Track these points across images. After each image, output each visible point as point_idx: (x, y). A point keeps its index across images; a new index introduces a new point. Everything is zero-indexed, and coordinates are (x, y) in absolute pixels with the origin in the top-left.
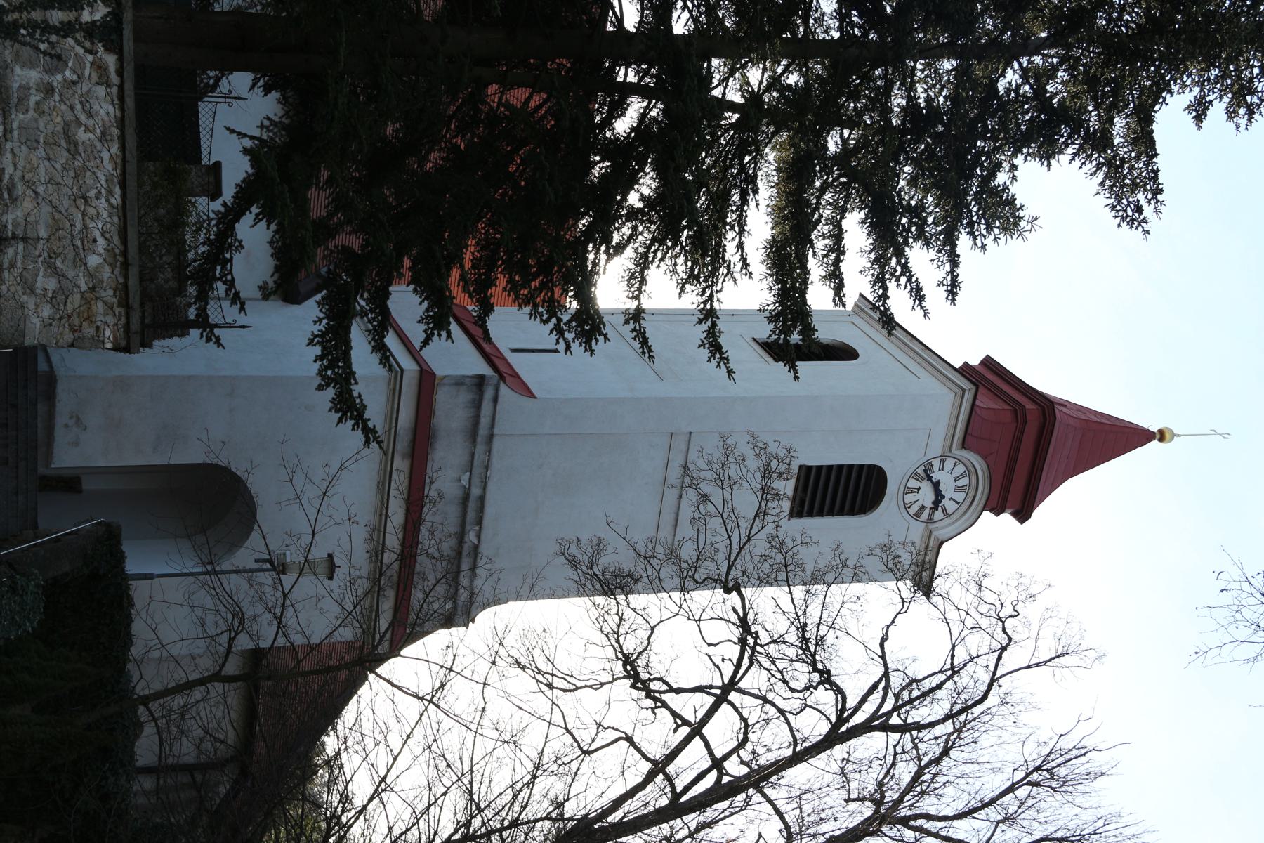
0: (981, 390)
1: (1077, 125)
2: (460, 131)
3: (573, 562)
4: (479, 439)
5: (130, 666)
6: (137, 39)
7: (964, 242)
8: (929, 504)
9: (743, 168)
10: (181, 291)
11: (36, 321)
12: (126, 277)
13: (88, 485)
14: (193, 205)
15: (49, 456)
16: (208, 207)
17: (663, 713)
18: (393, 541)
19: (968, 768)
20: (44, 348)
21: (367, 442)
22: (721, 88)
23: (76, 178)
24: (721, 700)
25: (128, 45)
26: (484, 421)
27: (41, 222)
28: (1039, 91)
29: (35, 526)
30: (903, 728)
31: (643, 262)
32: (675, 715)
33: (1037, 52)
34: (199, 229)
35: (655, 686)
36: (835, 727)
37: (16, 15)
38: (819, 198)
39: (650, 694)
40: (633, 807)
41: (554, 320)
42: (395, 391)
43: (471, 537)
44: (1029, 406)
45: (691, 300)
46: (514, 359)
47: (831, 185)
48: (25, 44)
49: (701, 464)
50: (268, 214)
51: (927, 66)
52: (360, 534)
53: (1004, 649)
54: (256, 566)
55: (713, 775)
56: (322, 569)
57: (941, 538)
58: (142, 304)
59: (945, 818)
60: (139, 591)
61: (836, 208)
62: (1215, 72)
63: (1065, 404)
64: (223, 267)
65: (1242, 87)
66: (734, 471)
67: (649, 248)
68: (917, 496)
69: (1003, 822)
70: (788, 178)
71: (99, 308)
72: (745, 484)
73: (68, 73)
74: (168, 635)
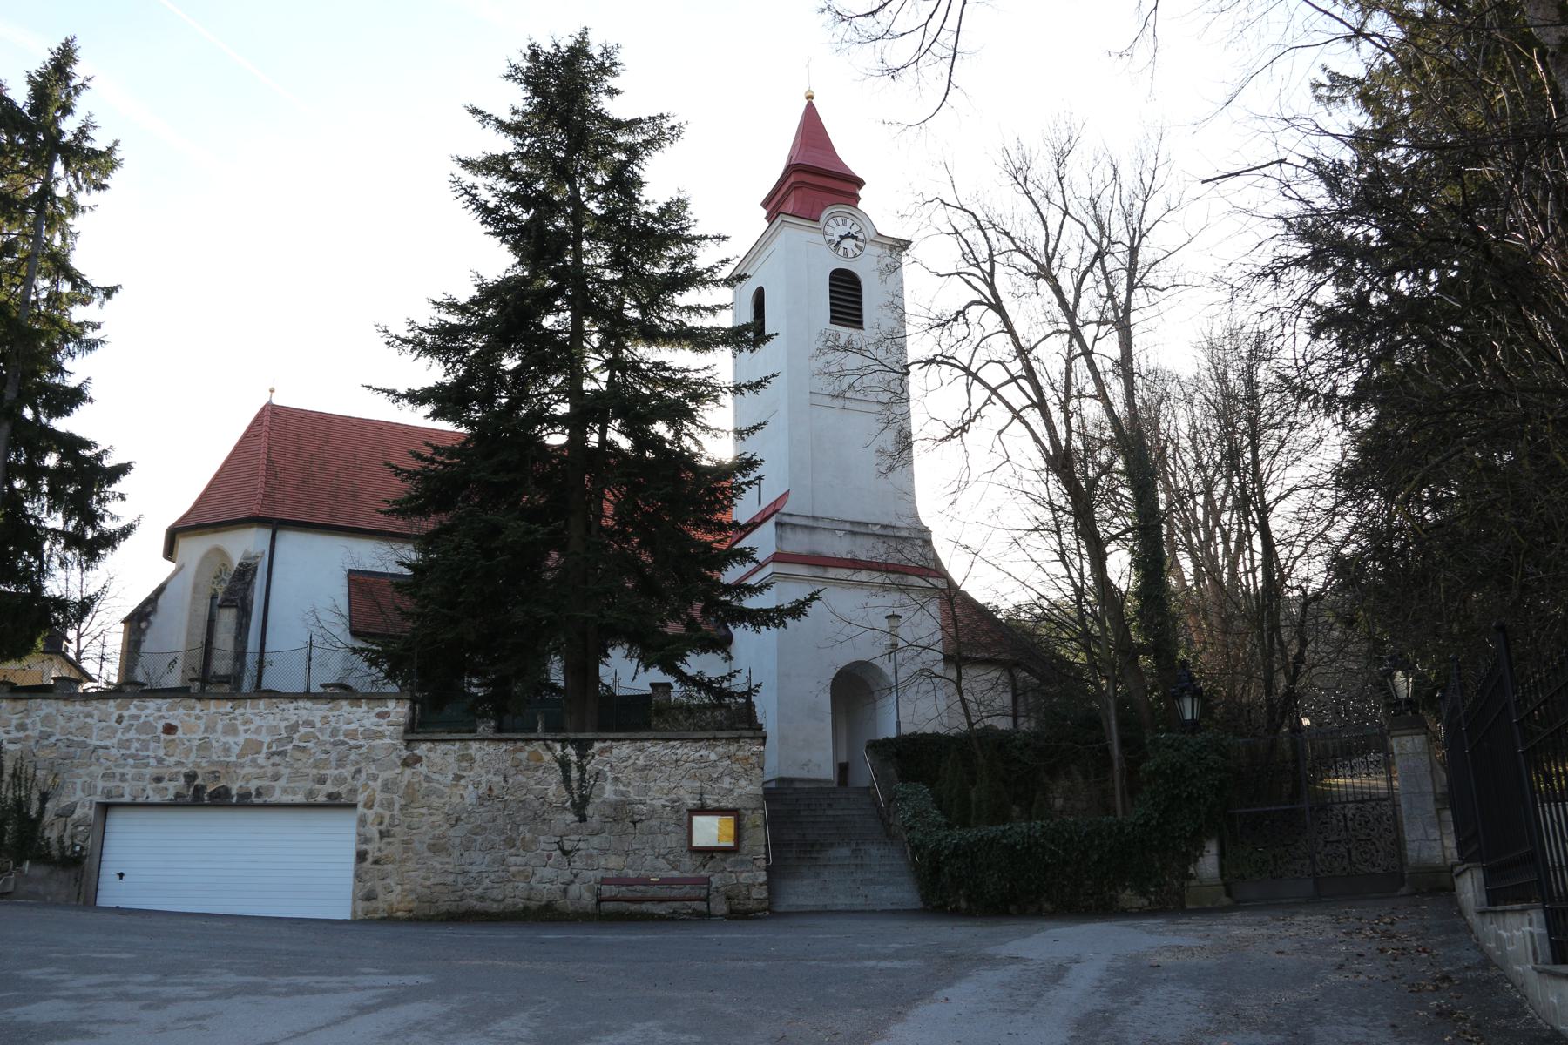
0: (782, 209)
1: (624, 165)
2: (629, 542)
3: (891, 469)
4: (815, 525)
5: (951, 734)
6: (584, 731)
7: (693, 232)
8: (854, 242)
9: (650, 370)
10: (728, 707)
11: (748, 788)
12: (722, 739)
13: (843, 759)
14: (676, 699)
15: (827, 781)
16: (677, 690)
17: (983, 412)
18: (877, 577)
19: (1017, 220)
20: (764, 783)
21: (818, 599)
22: (601, 384)
23: (665, 766)
24: (975, 377)
25: (588, 736)
26: (804, 522)
27: (692, 785)
28: (601, 189)
29: (868, 788)
30: (991, 260)
31: (705, 428)
32: (985, 404)
33: (578, 191)
34: (691, 696)
35: (967, 417)
36: (990, 306)
37: (575, 796)
38: (666, 322)
39: (972, 420)
40: (1041, 430)
41: (743, 486)
42: (786, 577)
43: (876, 529)
44: (792, 180)
45: (727, 399)
46: (765, 503)
47: (658, 314)
48: (591, 792)
49: (831, 388)
50: (682, 657)
51: (585, 257)
52: (874, 601)
53: (942, 202)
54: (892, 663)
55: (1021, 381)
56: (894, 622)
58: (737, 730)
59: (1047, 235)
60: (907, 729)
61: (672, 310)
62: (591, 85)
63: (791, 158)
64: (714, 682)
65: (600, 69)
66: (834, 369)
67: (698, 426)
69: (1048, 199)
70: (655, 342)
71: (740, 754)
72: (842, 362)
73: (606, 769)
74: (932, 713)
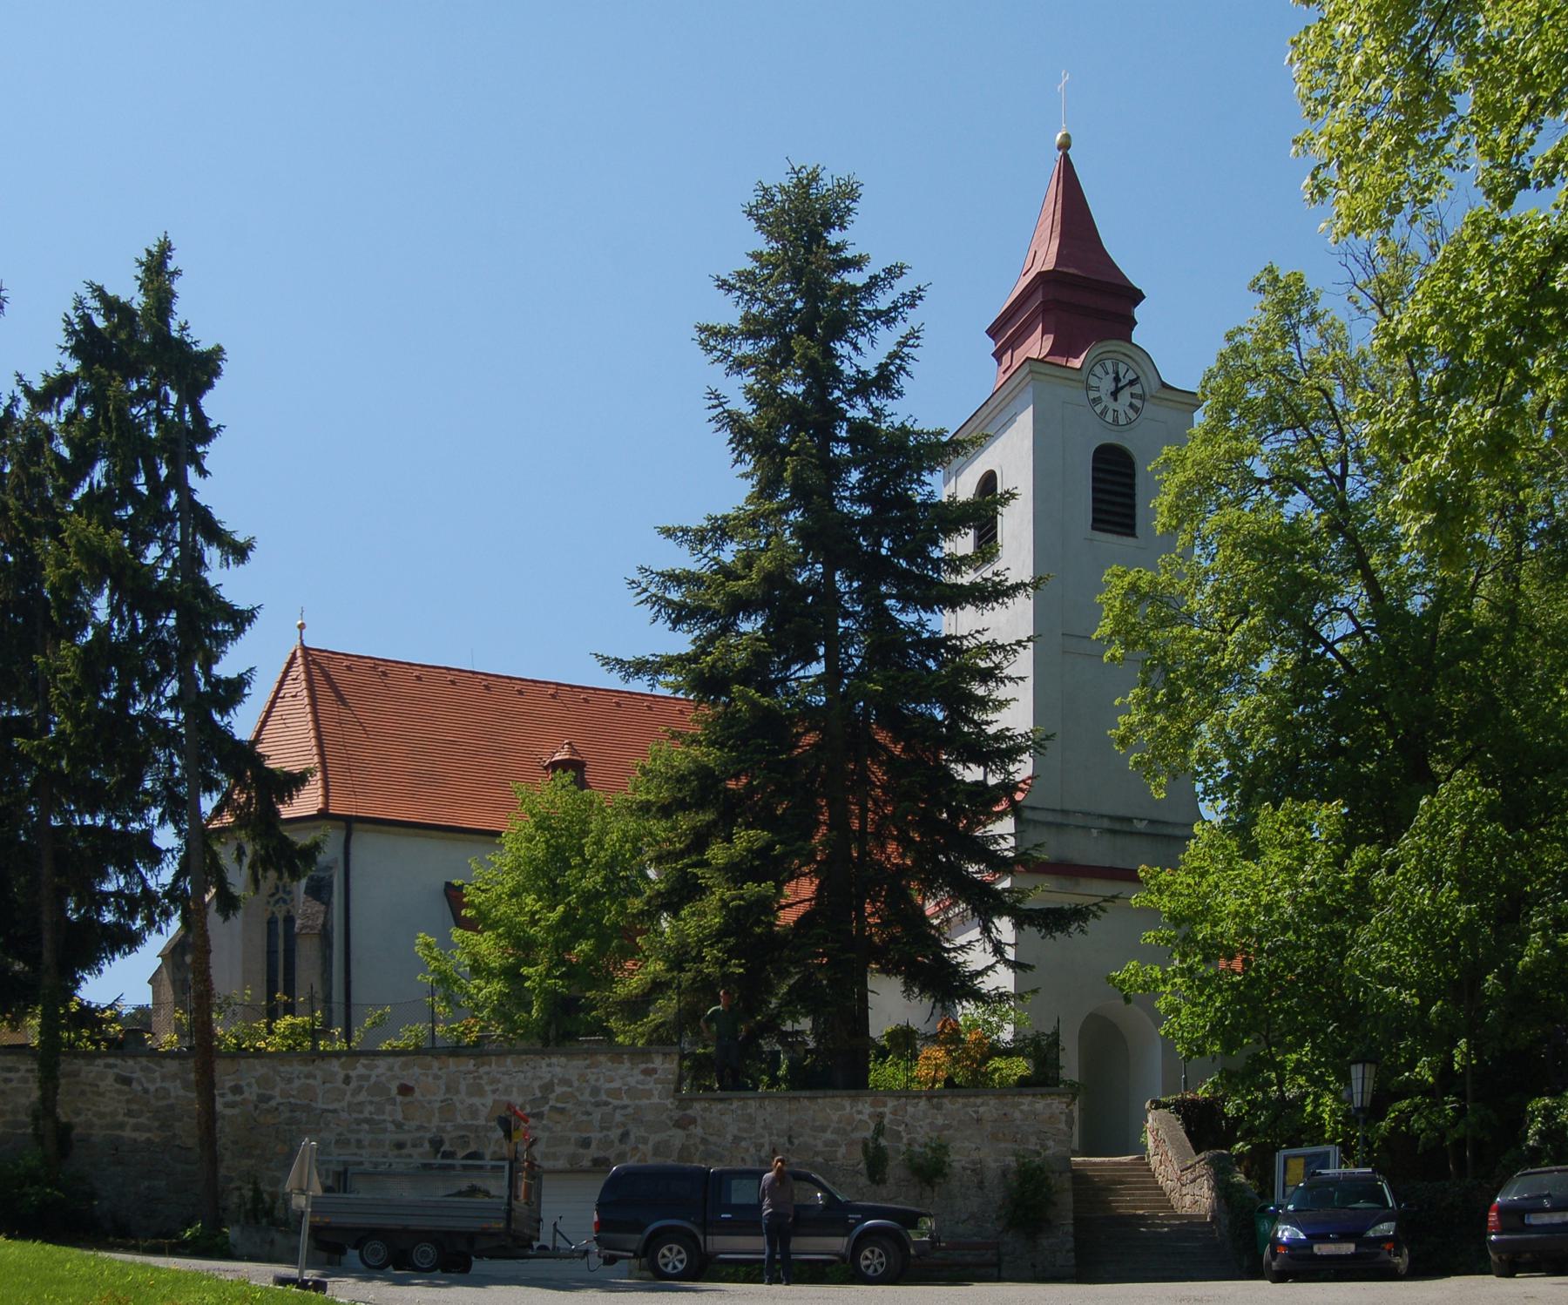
26: (1050, 818)
57: (1158, 385)
68: (1121, 411)
